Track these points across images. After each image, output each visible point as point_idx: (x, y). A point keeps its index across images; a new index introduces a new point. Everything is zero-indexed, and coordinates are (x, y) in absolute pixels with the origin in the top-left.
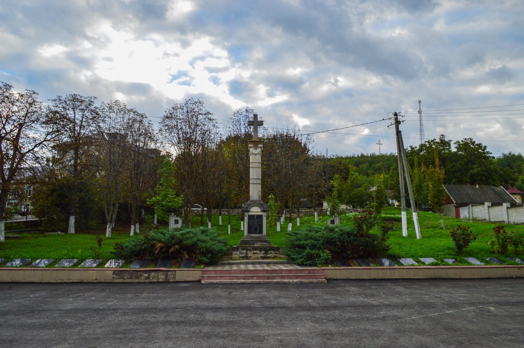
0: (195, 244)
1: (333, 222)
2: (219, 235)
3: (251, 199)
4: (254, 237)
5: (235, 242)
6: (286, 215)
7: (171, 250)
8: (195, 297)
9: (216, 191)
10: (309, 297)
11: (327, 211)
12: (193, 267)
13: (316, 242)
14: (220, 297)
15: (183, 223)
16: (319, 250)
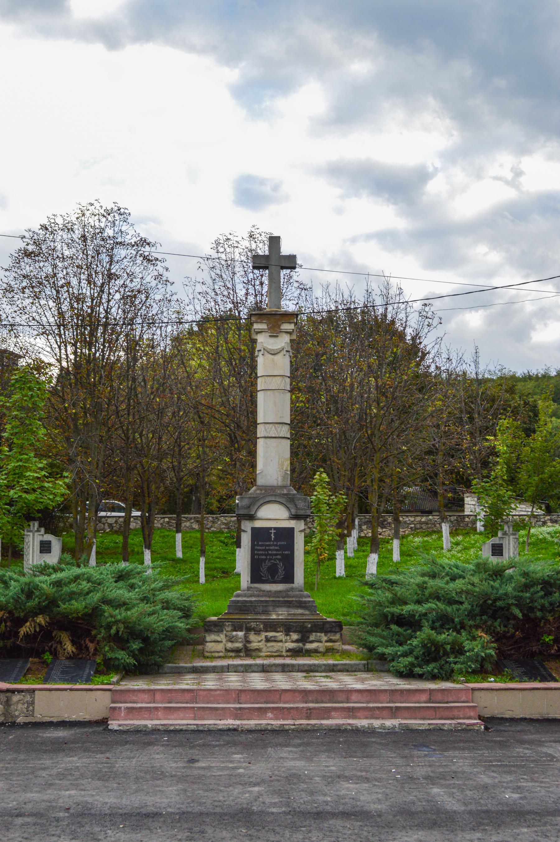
0: (94, 613)
1: (497, 550)
2: (167, 587)
3: (260, 481)
4: (269, 593)
5: (211, 607)
6: (361, 530)
7: (26, 629)
8: (82, 776)
9: (166, 464)
10: (431, 780)
11: (474, 522)
12: (88, 680)
13: (449, 609)
14: (158, 775)
15: (64, 550)
16: (459, 632)
